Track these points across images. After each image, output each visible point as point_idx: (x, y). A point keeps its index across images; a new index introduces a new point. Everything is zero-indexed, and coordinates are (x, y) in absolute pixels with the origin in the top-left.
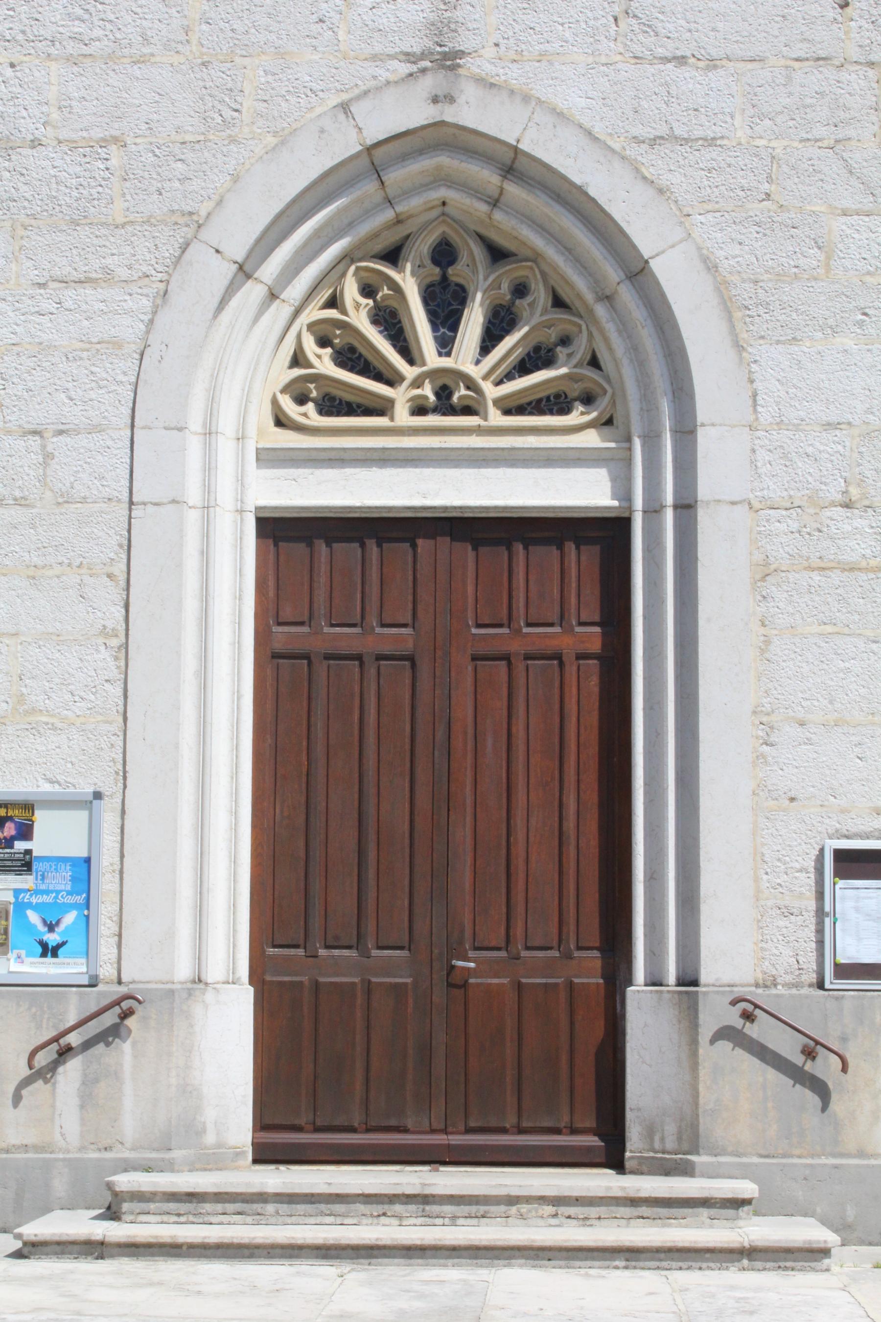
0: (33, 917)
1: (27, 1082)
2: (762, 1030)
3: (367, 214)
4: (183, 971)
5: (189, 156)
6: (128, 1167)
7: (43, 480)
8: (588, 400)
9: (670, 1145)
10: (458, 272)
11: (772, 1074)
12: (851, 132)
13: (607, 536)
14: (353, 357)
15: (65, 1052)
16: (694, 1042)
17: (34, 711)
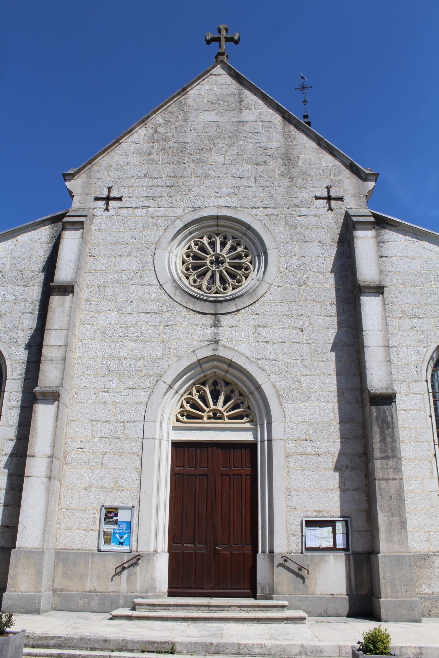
0: (117, 536)
3: (198, 374)
4: (152, 549)
5: (159, 361)
6: (138, 597)
8: (247, 416)
9: (267, 592)
10: (218, 387)
11: (291, 575)
12: (305, 358)
13: (251, 447)
14: (194, 406)
15: (124, 569)
16: (273, 567)
17: (119, 486)
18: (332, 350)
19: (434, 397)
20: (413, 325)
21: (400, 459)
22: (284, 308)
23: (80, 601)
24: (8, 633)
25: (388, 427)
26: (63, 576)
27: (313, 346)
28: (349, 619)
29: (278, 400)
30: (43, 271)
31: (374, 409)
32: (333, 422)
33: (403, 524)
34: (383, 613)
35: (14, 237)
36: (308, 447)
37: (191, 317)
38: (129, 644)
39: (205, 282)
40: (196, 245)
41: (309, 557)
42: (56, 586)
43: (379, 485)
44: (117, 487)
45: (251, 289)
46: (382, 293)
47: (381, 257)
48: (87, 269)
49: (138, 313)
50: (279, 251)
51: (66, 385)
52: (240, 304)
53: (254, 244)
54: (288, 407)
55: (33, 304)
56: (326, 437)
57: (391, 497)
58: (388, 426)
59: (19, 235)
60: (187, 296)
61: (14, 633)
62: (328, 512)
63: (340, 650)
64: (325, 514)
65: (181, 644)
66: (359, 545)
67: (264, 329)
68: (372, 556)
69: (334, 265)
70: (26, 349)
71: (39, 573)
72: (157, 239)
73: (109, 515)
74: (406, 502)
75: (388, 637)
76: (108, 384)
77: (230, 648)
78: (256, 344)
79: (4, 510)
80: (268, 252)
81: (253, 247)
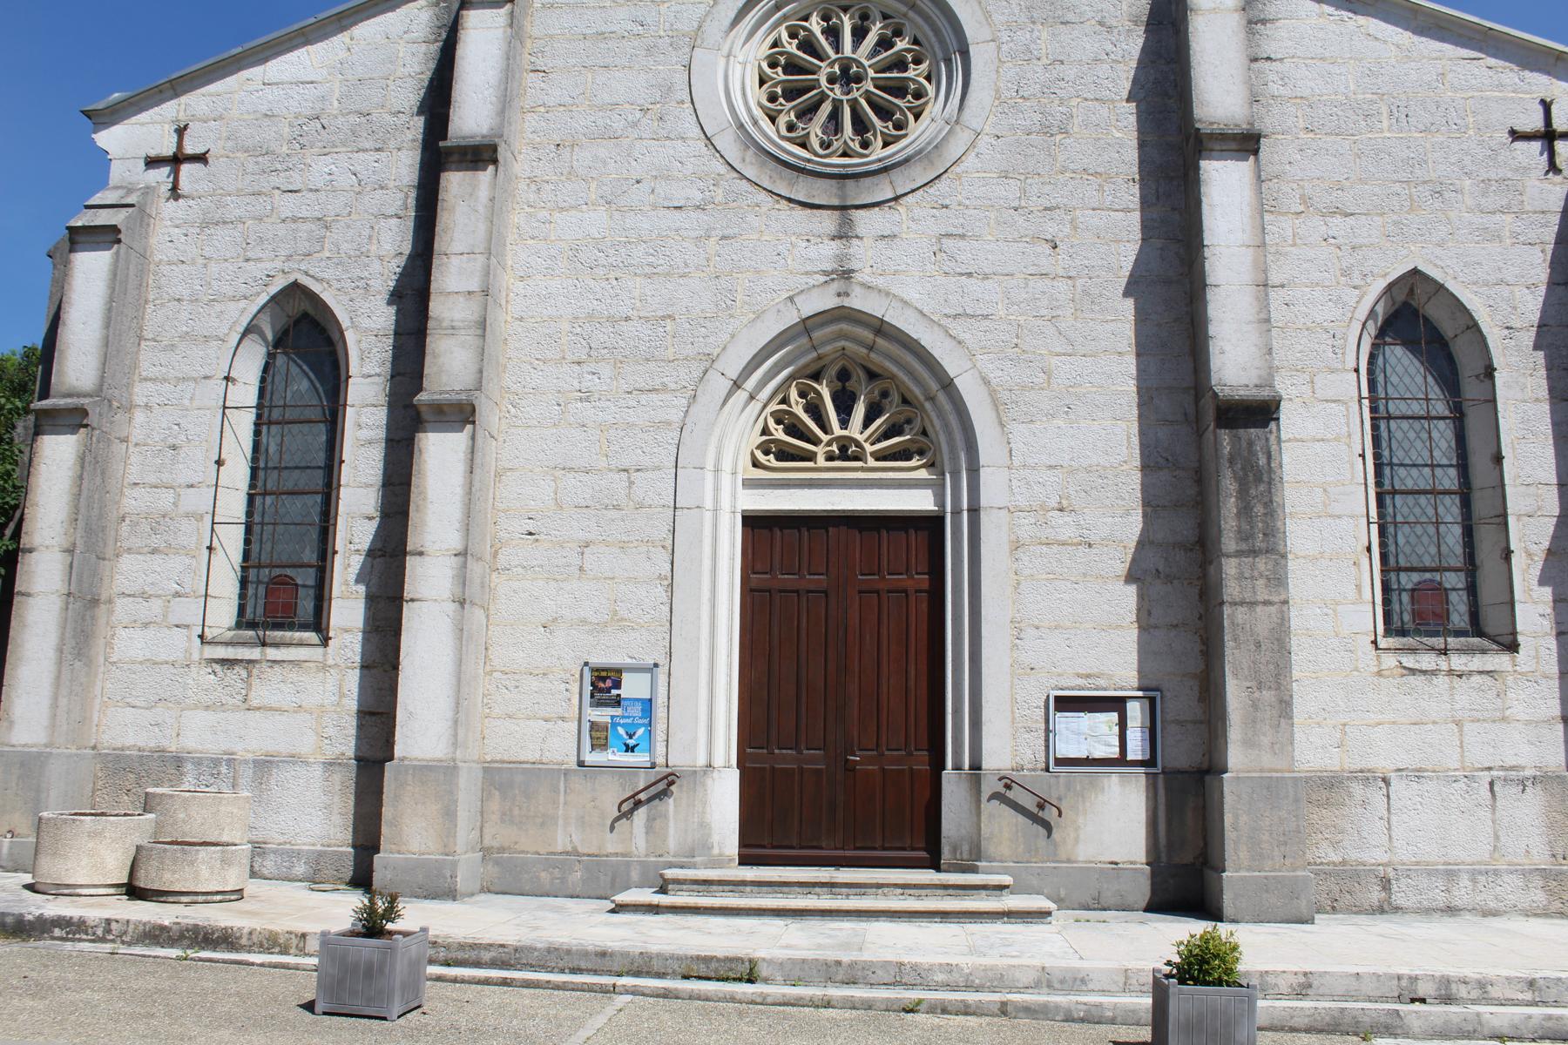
0: (621, 730)
1: (617, 819)
2: (1015, 794)
3: (803, 354)
4: (701, 761)
5: (708, 324)
6: (671, 866)
7: (628, 496)
8: (921, 453)
9: (965, 856)
10: (850, 385)
11: (1021, 818)
12: (1059, 312)
13: (929, 527)
14: (795, 429)
15: (638, 804)
16: (978, 801)
17: (622, 619)
18: (1126, 294)
19: (1373, 410)
20: (1331, 233)
21: (1284, 556)
22: (1010, 191)
23: (543, 875)
24: (391, 933)
25: (1258, 480)
26: (503, 821)
27: (1079, 282)
28: (1149, 915)
29: (994, 415)
30: (419, 113)
31: (1225, 437)
32: (1125, 467)
33: (1285, 706)
34: (1228, 903)
35: (343, 29)
36: (1065, 527)
37: (783, 215)
38: (654, 962)
39: (815, 129)
40: (793, 35)
41: (1062, 780)
42: (487, 842)
43: (1231, 616)
44: (617, 621)
45: (929, 143)
46: (1256, 152)
47: (1256, 60)
48: (527, 103)
49: (654, 207)
50: (999, 48)
51: (491, 387)
52: (902, 181)
53: (937, 32)
54: (1018, 431)
55: (402, 195)
56: (1108, 502)
57: (1258, 645)
58: (1259, 479)
59: (356, 24)
60: (773, 164)
61: (406, 934)
62: (1110, 677)
63: (1127, 978)
64: (1102, 682)
65: (770, 962)
66: (1179, 755)
67: (962, 244)
68: (1208, 778)
69: (1135, 81)
70: (389, 303)
71: (450, 814)
72: (696, 25)
73: (601, 685)
74: (1293, 657)
75: (1235, 948)
76: (589, 382)
77: (879, 972)
78: (941, 279)
79: (361, 678)
80: (972, 49)
81: (933, 39)
